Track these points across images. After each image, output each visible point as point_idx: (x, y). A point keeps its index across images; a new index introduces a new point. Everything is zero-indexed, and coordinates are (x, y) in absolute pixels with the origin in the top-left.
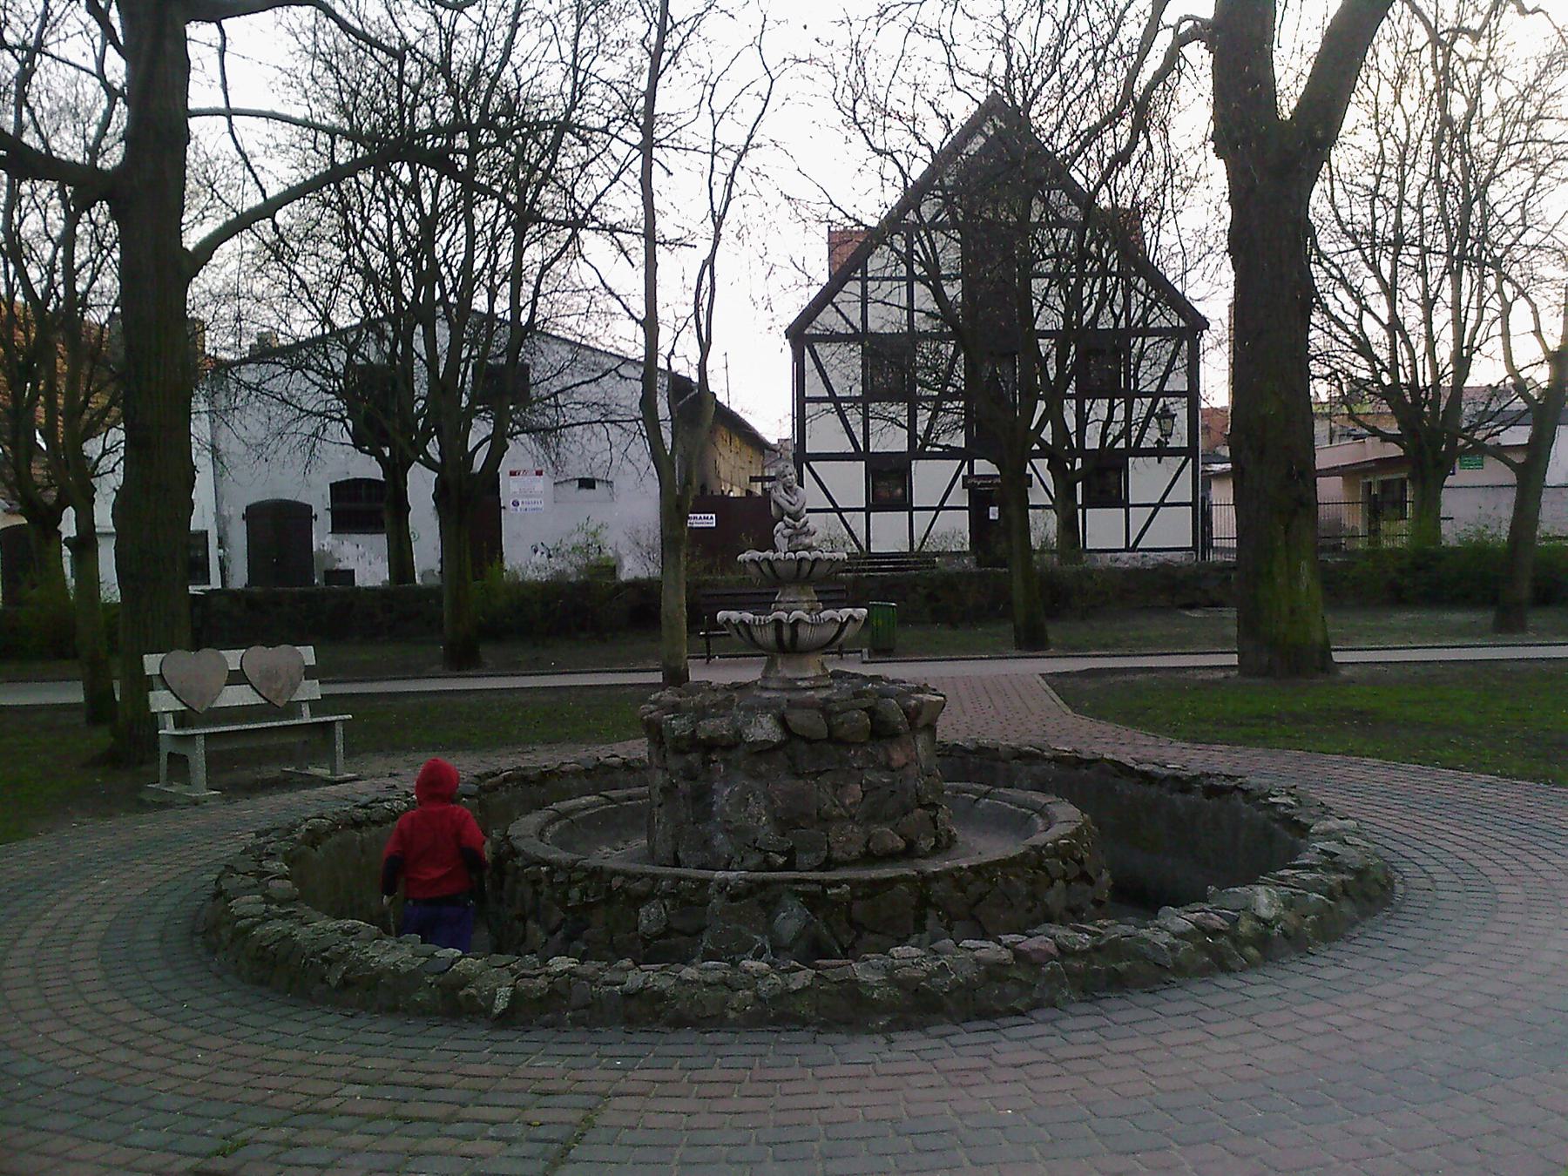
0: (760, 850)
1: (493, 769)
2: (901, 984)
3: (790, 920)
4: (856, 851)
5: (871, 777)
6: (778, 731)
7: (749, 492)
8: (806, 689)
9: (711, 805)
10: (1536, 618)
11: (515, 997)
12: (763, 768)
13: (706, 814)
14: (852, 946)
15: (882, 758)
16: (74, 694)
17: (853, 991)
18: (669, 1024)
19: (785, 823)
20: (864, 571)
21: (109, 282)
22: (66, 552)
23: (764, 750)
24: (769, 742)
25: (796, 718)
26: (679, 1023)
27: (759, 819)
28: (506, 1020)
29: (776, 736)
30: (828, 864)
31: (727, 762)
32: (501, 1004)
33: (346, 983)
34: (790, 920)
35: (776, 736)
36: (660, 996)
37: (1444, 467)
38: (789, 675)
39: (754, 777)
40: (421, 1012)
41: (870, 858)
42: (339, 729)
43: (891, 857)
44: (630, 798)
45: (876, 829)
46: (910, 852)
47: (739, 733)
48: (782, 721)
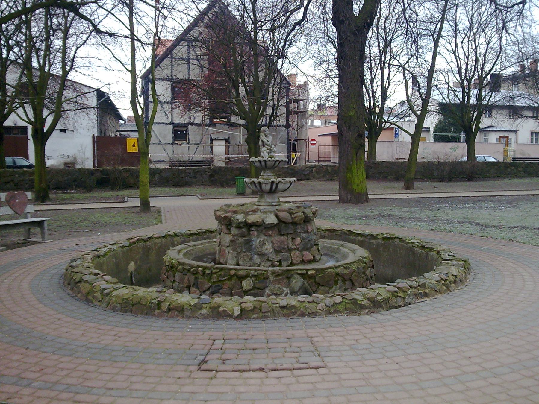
0: (270, 260)
1: (130, 236)
2: (369, 299)
3: (297, 282)
4: (299, 259)
5: (304, 235)
6: (277, 220)
7: (116, 135)
8: (276, 205)
9: (252, 246)
10: (417, 184)
11: (242, 310)
12: (270, 233)
13: (249, 249)
14: (316, 290)
15: (306, 229)
16: (136, 203)
17: (354, 302)
18: (299, 315)
19: (277, 251)
20: (187, 166)
21: (370, 34)
22: (366, 140)
23: (271, 227)
24: (274, 223)
25: (281, 214)
26: (303, 315)
27: (270, 250)
28: (239, 317)
29: (276, 221)
30: (292, 264)
31: (257, 230)
32: (237, 312)
33: (169, 309)
34: (297, 282)
35: (276, 221)
36: (293, 307)
37: (378, 135)
38: (270, 201)
39: (267, 236)
40: (205, 317)
41: (303, 262)
42: (46, 224)
43: (309, 262)
44: (195, 246)
45: (305, 253)
46: (314, 261)
47: (263, 221)
48: (277, 216)
